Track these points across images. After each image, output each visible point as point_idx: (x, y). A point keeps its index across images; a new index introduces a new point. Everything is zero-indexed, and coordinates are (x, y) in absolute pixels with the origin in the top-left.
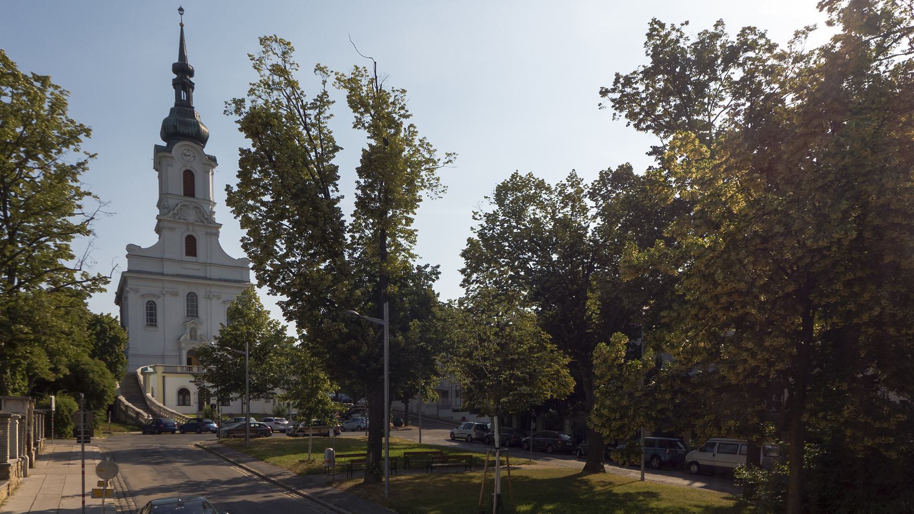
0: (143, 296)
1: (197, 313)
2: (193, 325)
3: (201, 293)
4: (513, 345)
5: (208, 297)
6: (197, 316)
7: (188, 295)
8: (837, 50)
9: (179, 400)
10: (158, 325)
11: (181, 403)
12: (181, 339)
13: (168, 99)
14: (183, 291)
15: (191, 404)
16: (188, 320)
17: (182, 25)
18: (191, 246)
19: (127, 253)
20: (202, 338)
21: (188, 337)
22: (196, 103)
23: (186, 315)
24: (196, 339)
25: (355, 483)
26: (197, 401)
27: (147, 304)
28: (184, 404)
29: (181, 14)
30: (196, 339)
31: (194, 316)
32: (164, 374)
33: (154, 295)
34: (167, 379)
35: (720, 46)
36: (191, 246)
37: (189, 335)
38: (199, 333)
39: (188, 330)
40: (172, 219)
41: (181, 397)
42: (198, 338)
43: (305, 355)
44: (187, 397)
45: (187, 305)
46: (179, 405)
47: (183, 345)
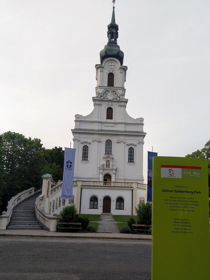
0: (128, 145)
1: (133, 160)
3: (114, 140)
5: (118, 142)
7: (106, 142)
10: (88, 160)
13: (105, 40)
14: (104, 139)
17: (114, 8)
18: (110, 114)
19: (75, 119)
22: (117, 42)
25: (59, 241)
27: (83, 148)
29: (114, 3)
32: (82, 187)
33: (133, 145)
34: (83, 190)
36: (110, 114)
40: (100, 99)
45: (111, 149)
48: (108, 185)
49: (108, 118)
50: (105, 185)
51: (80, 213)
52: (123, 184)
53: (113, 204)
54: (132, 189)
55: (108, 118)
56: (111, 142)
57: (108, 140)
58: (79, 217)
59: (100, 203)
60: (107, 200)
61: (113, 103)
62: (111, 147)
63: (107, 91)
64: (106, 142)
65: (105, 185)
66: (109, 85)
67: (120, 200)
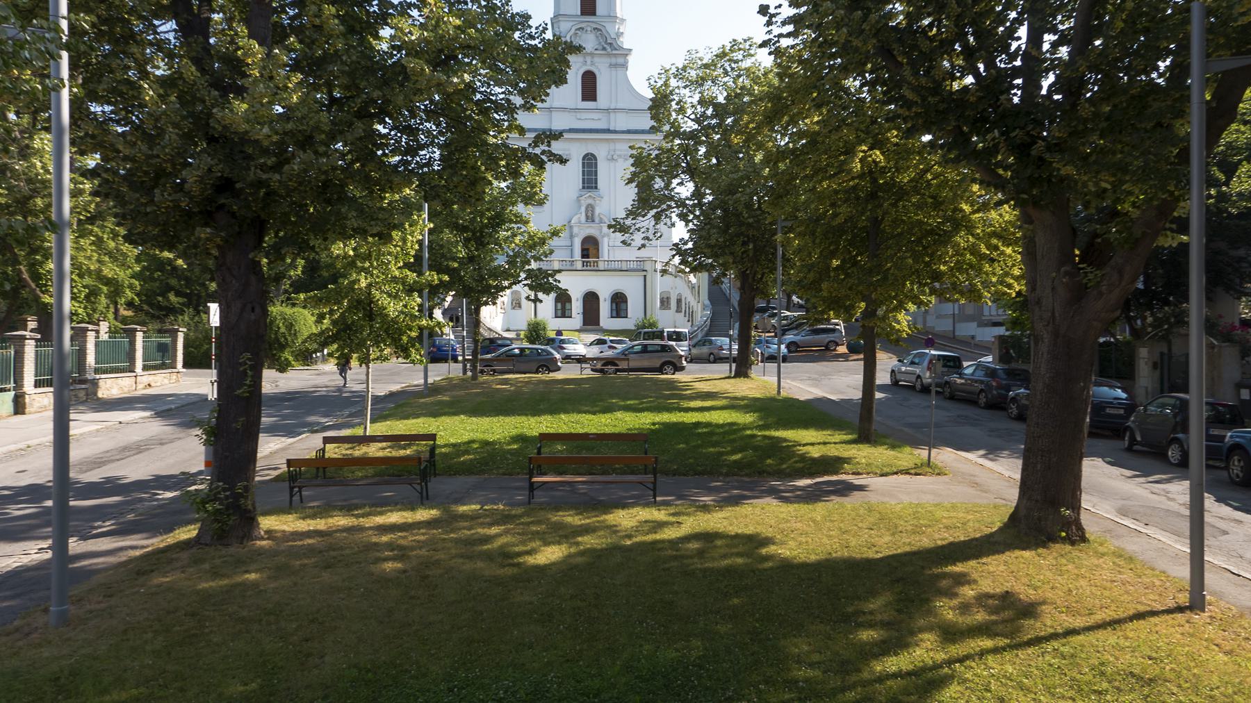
1: (596, 183)
2: (590, 201)
6: (596, 188)
9: (556, 310)
11: (614, 315)
24: (593, 221)
28: (618, 316)
30: (593, 221)
31: (591, 188)
37: (584, 214)
38: (597, 211)
39: (583, 209)
41: (559, 306)
42: (597, 220)
44: (568, 306)
47: (575, 230)
48: (592, 268)
49: (585, 98)
50: (53, 106)
51: (779, 392)
52: (624, 263)
53: (605, 308)
54: (644, 273)
55: (585, 98)
56: (596, 159)
57: (587, 155)
58: (122, 231)
59: (577, 307)
60: (591, 299)
61: (596, 59)
62: (596, 172)
63: (579, 29)
64: (584, 159)
66: (584, 13)
67: (619, 301)
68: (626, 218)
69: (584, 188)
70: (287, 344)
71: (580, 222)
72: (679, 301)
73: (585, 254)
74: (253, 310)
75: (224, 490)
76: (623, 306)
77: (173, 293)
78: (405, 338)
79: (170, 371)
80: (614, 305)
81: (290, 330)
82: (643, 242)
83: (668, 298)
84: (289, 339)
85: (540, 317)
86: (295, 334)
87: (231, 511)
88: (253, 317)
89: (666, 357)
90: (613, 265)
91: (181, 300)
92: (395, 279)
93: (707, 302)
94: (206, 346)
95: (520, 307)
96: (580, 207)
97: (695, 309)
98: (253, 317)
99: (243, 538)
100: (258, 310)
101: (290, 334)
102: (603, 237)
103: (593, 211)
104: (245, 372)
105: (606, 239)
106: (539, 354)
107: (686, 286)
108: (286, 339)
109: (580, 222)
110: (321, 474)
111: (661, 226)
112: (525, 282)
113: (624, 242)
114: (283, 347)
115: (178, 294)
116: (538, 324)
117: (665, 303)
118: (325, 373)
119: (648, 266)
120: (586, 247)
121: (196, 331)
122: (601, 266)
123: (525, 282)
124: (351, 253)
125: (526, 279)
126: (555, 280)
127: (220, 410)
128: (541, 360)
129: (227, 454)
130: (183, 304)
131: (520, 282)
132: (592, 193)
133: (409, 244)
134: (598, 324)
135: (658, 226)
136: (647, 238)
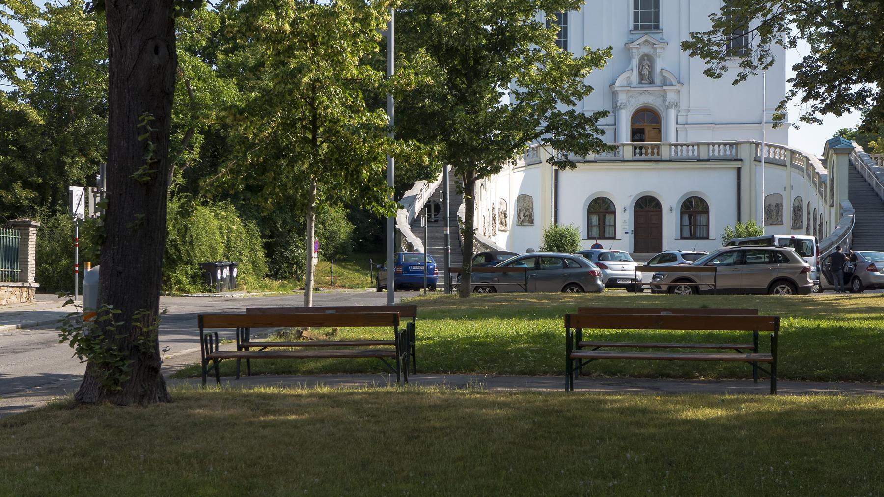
1: (657, 18)
2: (646, 50)
4: (135, 228)
6: (657, 27)
8: (389, 118)
9: (590, 226)
11: (687, 233)
12: (617, 84)
15: (618, 236)
16: (635, 37)
20: (664, 78)
21: (635, 77)
23: (631, 27)
24: (652, 82)
26: (630, 227)
28: (693, 236)
30: (652, 82)
31: (648, 28)
35: (384, 105)
37: (635, 72)
38: (659, 65)
39: (635, 62)
41: (595, 219)
42: (658, 80)
43: (82, 241)
44: (609, 218)
46: (682, 238)
47: (622, 98)
48: (649, 157)
54: (738, 165)
59: (624, 221)
65: (638, 157)
68: (713, 32)
69: (636, 28)
70: (179, 257)
71: (629, 85)
72: (797, 210)
73: (637, 134)
74: (156, 51)
75: (117, 317)
76: (701, 219)
77: (19, 183)
78: (365, 174)
79: (20, 284)
80: (686, 218)
81: (184, 236)
82: (741, 70)
83: (779, 206)
84: (183, 249)
85: (565, 223)
86: (191, 243)
87: (126, 353)
88: (156, 61)
89: (780, 270)
90: (684, 152)
91: (32, 195)
92: (349, 84)
93: (847, 204)
94: (65, 262)
95: (531, 221)
96: (630, 59)
97: (826, 218)
98: (156, 61)
99: (143, 397)
100: (163, 50)
101: (184, 243)
102: (668, 108)
103: (652, 67)
104: (146, 147)
105: (673, 113)
106: (565, 266)
107: (809, 184)
108: (179, 251)
109: (629, 85)
110: (244, 367)
111: (772, 46)
112: (547, 136)
113: (709, 73)
114: (173, 263)
115: (26, 185)
116: (562, 235)
117: (773, 213)
118: (236, 300)
119: (744, 153)
120: (639, 126)
121: (51, 239)
122: (665, 153)
123: (547, 136)
124: (287, 28)
125: (548, 130)
126: (597, 130)
127: (109, 204)
128: (570, 275)
129: (120, 268)
130: (33, 200)
131: (537, 136)
132: (652, 37)
133: (373, 23)
134: (659, 247)
135: (766, 47)
136: (749, 64)
